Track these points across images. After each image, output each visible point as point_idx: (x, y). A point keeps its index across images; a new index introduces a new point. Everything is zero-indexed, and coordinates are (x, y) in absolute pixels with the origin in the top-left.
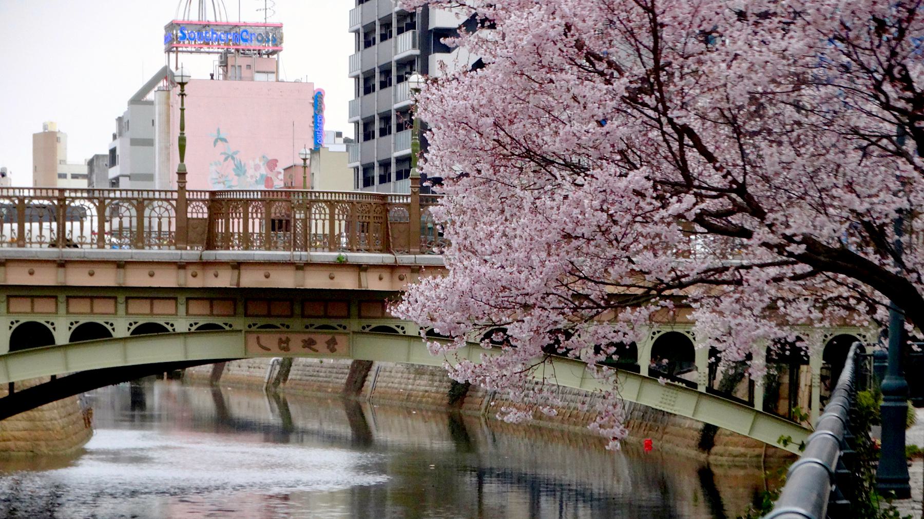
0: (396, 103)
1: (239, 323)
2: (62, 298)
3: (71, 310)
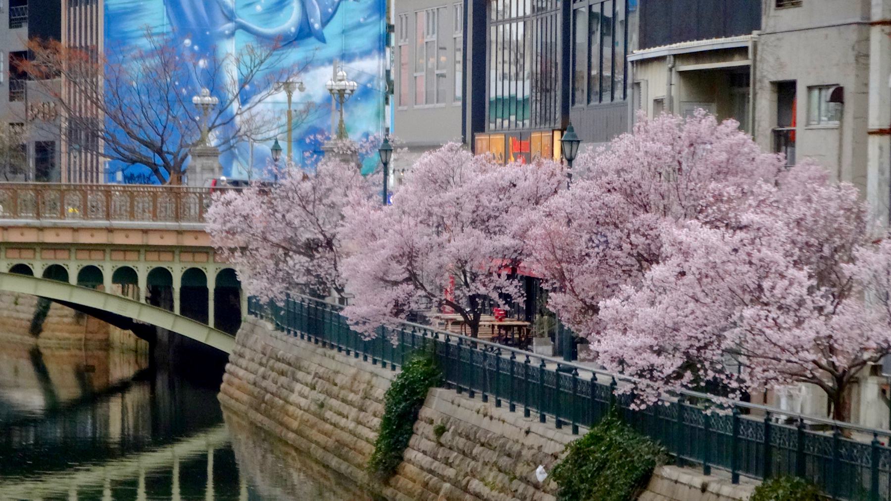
2: (177, 252)
3: (113, 258)
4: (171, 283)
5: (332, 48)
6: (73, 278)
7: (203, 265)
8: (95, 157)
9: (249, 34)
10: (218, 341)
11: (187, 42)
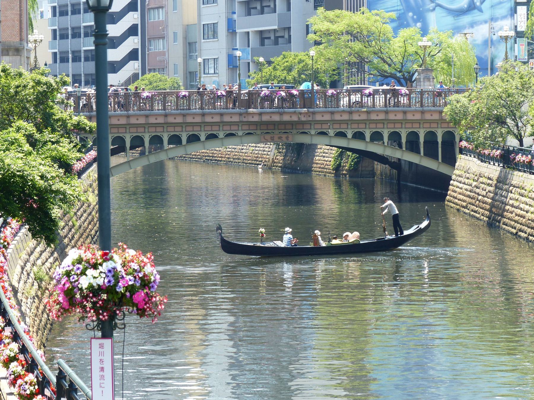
0: (83, 23)
1: (259, 132)
4: (419, 139)
5: (486, 15)
6: (368, 138)
7: (236, 132)
8: (363, 74)
9: (444, 10)
10: (444, 169)
11: (411, 14)
